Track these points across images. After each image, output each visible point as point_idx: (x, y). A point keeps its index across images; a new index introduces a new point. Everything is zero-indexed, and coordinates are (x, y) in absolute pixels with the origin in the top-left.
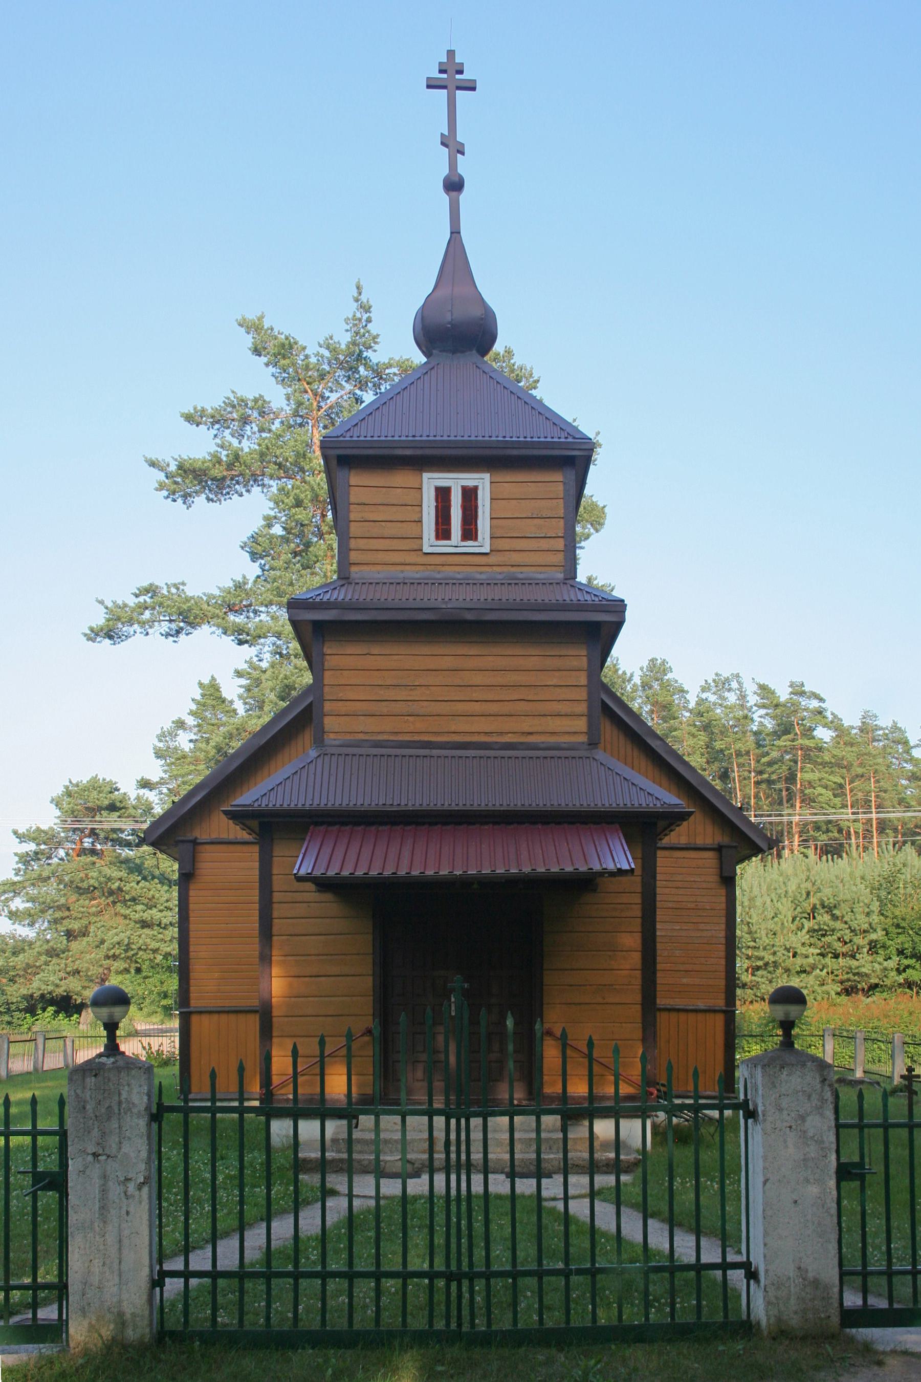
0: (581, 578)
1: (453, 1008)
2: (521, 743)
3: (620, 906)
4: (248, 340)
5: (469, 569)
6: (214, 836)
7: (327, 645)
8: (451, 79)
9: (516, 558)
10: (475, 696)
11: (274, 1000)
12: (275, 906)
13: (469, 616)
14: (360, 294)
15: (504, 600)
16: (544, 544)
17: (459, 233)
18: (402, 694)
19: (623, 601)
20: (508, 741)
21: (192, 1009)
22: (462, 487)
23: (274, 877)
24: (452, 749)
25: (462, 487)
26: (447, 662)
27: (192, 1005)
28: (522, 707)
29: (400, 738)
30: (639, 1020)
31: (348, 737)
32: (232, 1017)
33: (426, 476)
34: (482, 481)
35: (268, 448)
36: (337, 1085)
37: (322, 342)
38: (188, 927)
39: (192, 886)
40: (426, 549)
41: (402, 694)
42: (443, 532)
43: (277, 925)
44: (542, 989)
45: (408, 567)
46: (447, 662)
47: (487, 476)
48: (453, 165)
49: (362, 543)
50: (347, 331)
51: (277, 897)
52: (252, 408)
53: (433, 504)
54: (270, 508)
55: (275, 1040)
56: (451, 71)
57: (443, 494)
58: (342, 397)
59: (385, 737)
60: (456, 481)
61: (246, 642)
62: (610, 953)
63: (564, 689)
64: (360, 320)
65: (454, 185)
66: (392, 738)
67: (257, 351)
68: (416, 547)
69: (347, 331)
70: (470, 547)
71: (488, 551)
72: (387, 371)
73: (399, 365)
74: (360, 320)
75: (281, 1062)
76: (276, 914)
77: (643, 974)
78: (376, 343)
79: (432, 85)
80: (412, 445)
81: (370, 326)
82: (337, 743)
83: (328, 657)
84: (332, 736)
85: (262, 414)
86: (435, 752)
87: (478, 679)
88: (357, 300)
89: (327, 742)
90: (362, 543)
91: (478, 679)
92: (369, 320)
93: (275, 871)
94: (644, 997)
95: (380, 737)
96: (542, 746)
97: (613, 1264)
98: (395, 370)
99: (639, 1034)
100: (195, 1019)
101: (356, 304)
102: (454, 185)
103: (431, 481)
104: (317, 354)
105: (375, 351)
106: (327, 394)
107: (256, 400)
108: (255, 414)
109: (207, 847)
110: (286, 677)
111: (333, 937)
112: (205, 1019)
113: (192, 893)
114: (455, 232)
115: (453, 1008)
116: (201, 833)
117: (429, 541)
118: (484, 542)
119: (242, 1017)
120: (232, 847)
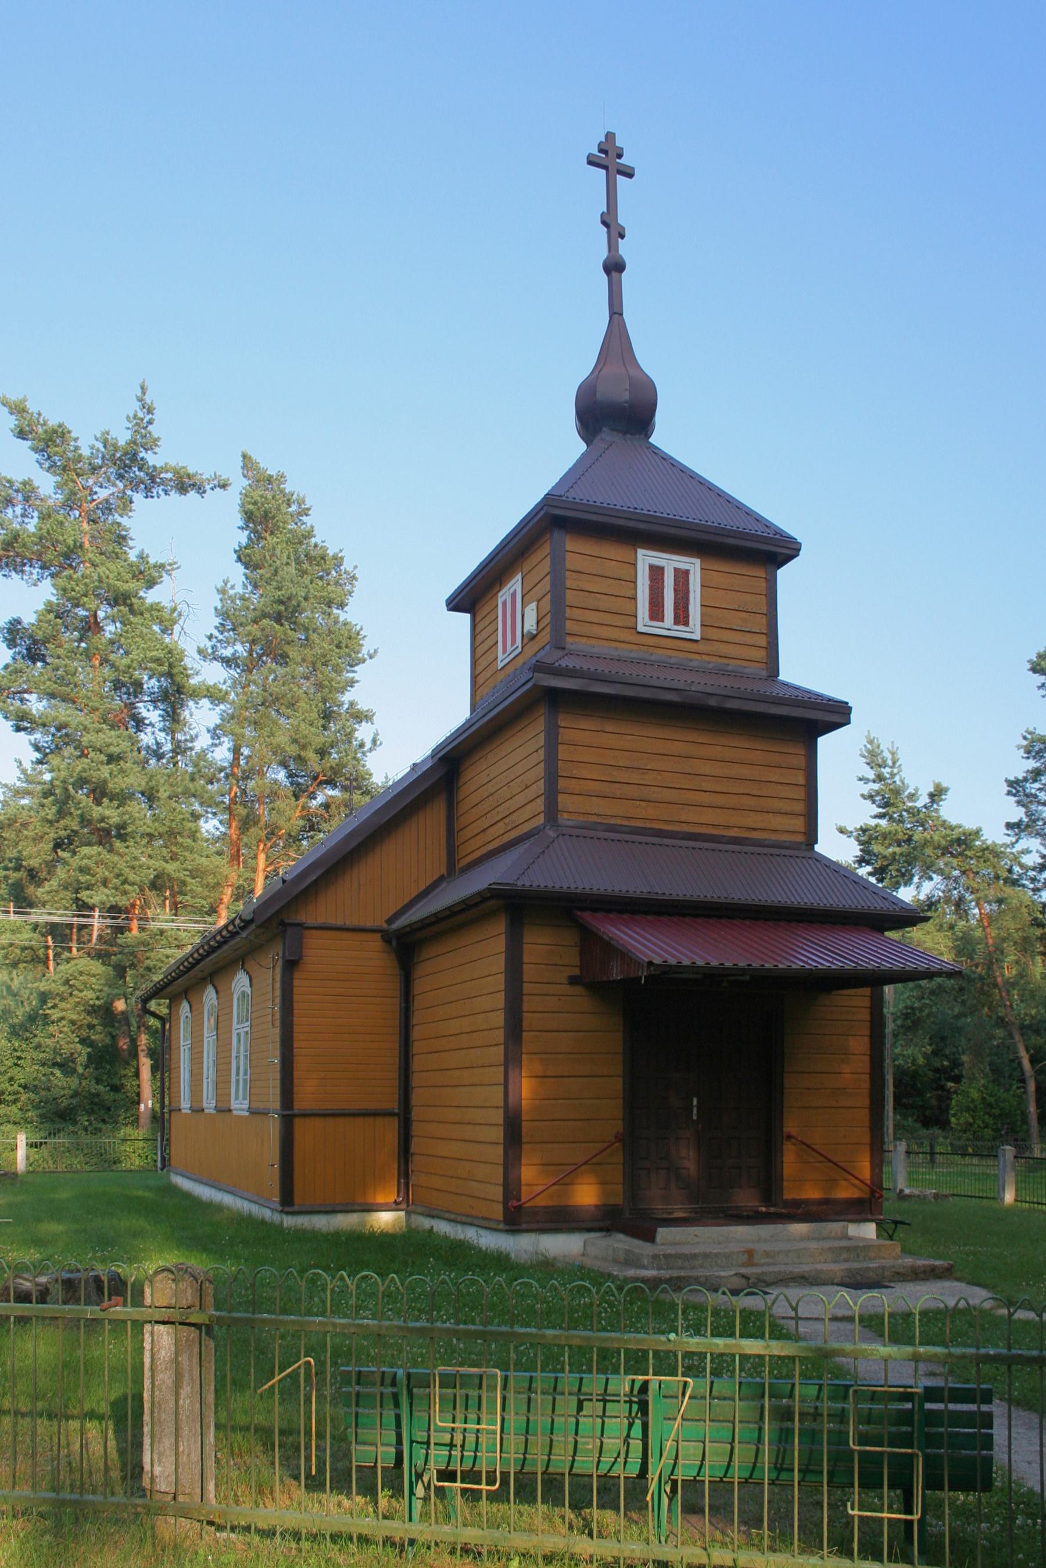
0: (783, 676)
1: (695, 1112)
2: (746, 838)
3: (854, 1009)
4: (12, 421)
5: (681, 655)
6: (321, 920)
7: (561, 717)
8: (609, 159)
9: (724, 649)
10: (705, 786)
11: (523, 1102)
12: (525, 997)
13: (713, 702)
14: (144, 393)
15: (742, 689)
16: (748, 639)
17: (621, 314)
18: (635, 778)
19: (847, 703)
20: (735, 835)
21: (296, 1111)
22: (675, 569)
23: (525, 966)
24: (684, 839)
25: (675, 569)
26: (678, 748)
27: (296, 1107)
28: (747, 801)
29: (633, 823)
30: (867, 1124)
31: (581, 818)
32: (330, 1121)
33: (641, 552)
34: (693, 565)
35: (48, 533)
36: (586, 1195)
37: (99, 435)
38: (292, 1021)
39: (296, 975)
40: (641, 628)
41: (635, 778)
42: (656, 612)
43: (527, 1020)
44: (783, 1093)
45: (623, 645)
46: (678, 748)
47: (697, 562)
48: (612, 246)
49: (576, 613)
50: (128, 428)
51: (527, 988)
52: (17, 491)
53: (647, 582)
54: (52, 594)
55: (524, 1146)
56: (612, 154)
57: (657, 573)
58: (113, 494)
59: (618, 821)
60: (671, 562)
61: (25, 729)
62: (843, 1057)
63: (786, 787)
64: (142, 420)
65: (614, 267)
66: (625, 823)
67: (22, 434)
68: (630, 625)
69: (128, 428)
70: (680, 632)
71: (699, 638)
72: (162, 476)
73: (176, 472)
74: (142, 420)
75: (528, 1173)
76: (526, 1007)
77: (871, 1078)
78: (156, 445)
79: (592, 162)
80: (625, 516)
81: (150, 428)
82: (569, 823)
83: (561, 730)
84: (565, 815)
85: (27, 499)
86: (666, 841)
87: (707, 768)
88: (140, 400)
89: (560, 821)
90: (576, 613)
91: (707, 768)
92: (150, 422)
93: (525, 959)
94: (872, 1101)
95: (613, 821)
96: (767, 843)
97: (967, 1381)
98: (169, 475)
99: (867, 1139)
100: (298, 1122)
101: (139, 404)
102: (614, 267)
103: (646, 558)
104: (92, 447)
105: (155, 453)
106: (96, 489)
107: (25, 483)
108: (20, 497)
109: (313, 932)
110: (84, 770)
111: (582, 1034)
112: (311, 1122)
113: (296, 982)
114: (616, 311)
115: (695, 1112)
116: (308, 916)
117: (643, 622)
118: (694, 630)
119: (379, 1121)
120: (339, 934)
